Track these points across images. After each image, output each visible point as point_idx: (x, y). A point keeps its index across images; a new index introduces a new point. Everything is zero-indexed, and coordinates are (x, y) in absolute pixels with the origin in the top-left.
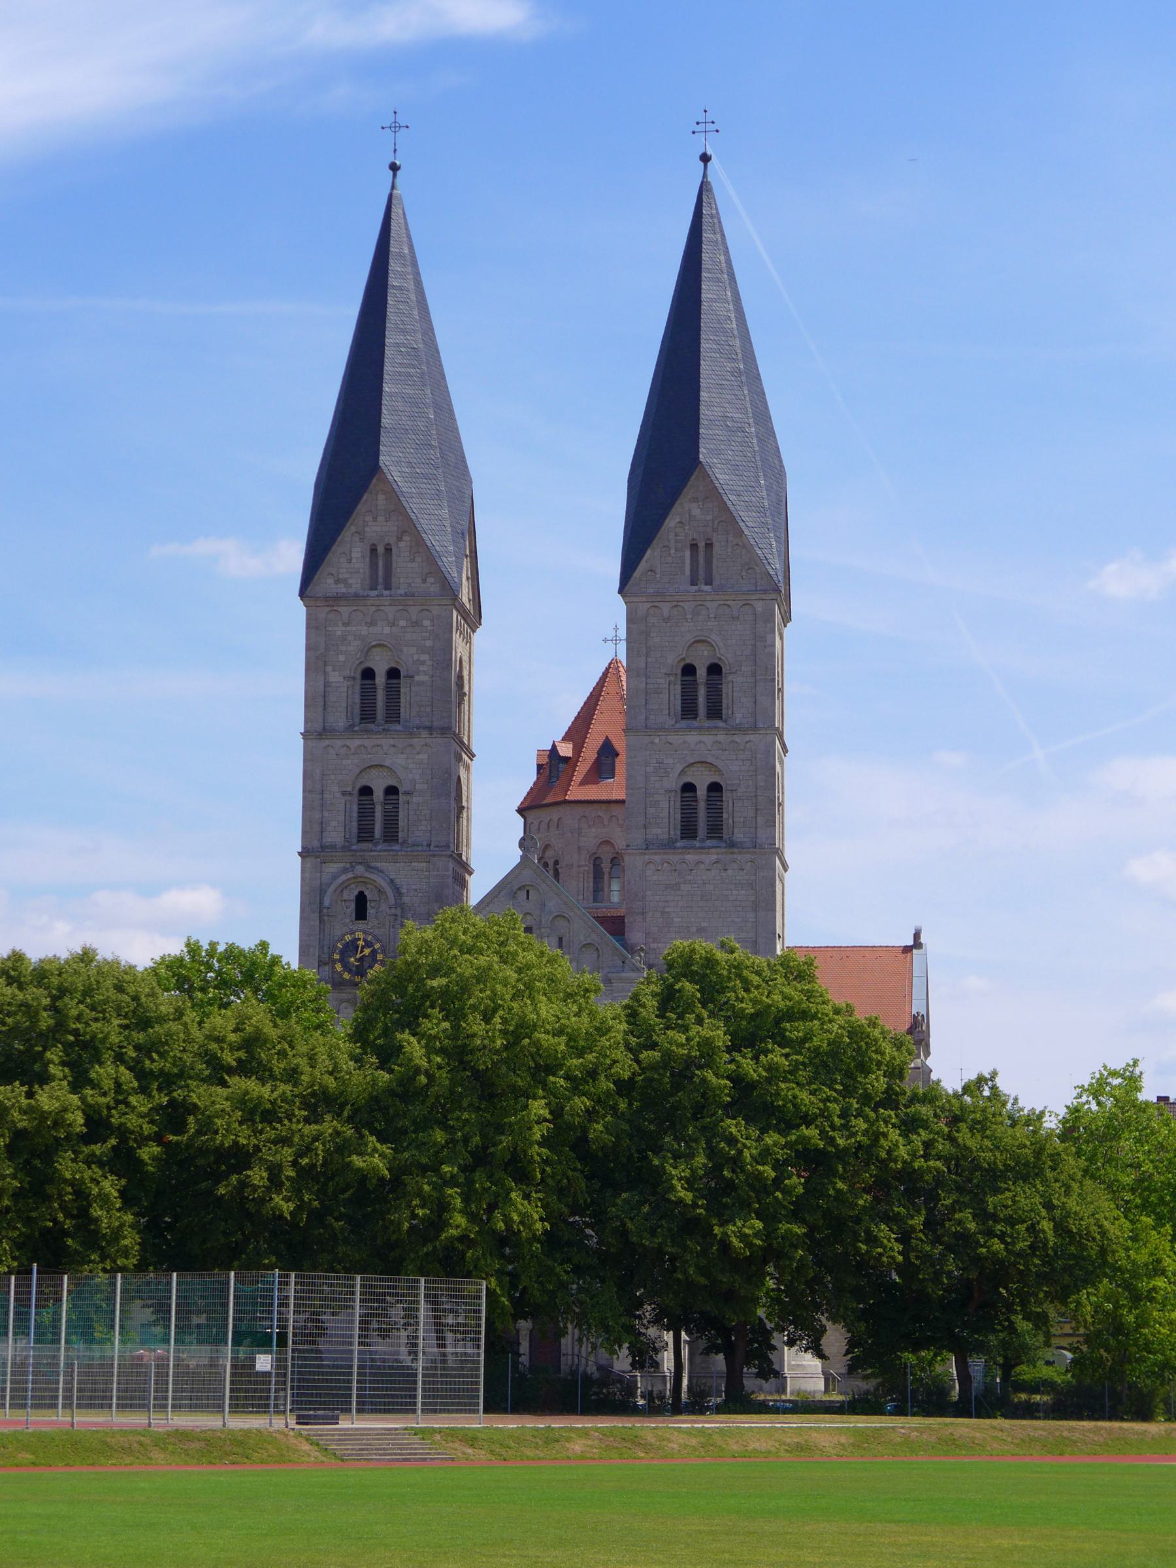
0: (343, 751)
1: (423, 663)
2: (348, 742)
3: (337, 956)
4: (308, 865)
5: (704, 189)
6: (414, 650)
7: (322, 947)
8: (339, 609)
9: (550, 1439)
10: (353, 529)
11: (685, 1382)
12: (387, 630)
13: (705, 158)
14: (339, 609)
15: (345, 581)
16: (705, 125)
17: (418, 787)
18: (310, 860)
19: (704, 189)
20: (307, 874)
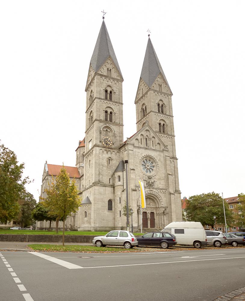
2: (104, 101)
12: (111, 83)
13: (149, 35)
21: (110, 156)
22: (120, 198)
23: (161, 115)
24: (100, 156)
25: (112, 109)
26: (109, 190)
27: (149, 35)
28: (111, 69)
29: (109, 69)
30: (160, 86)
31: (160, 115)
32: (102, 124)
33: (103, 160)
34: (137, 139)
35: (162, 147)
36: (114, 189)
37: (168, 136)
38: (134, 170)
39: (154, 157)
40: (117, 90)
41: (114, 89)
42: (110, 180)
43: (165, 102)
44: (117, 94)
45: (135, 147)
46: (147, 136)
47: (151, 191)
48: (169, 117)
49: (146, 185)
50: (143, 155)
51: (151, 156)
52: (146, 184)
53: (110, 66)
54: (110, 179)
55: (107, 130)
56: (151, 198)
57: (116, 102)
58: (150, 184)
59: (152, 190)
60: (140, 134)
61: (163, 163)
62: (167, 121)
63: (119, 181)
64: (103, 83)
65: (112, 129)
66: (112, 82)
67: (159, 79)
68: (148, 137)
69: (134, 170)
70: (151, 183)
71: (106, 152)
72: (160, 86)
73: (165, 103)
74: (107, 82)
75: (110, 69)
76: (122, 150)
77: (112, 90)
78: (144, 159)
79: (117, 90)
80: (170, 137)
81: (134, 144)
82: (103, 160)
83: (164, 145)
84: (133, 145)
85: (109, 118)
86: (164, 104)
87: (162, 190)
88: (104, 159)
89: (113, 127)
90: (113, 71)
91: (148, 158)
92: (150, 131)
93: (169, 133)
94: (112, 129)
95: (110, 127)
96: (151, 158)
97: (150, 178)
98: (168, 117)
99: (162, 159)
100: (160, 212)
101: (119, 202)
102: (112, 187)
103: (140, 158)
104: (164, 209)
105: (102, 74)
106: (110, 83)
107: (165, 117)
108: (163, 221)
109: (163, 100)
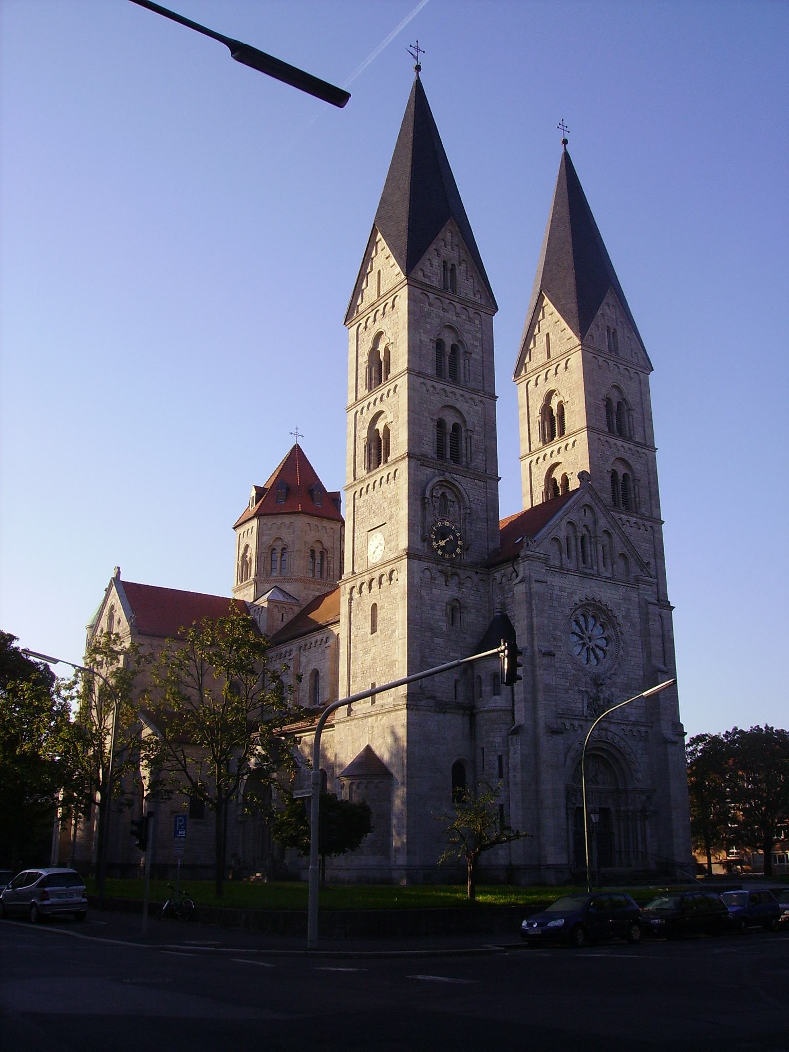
0: (431, 389)
1: (476, 347)
2: (435, 384)
3: (458, 550)
4: (413, 464)
5: (566, 156)
6: (470, 336)
7: (423, 528)
8: (429, 294)
9: (366, 618)
10: (434, 247)
11: (448, 664)
12: (455, 318)
13: (565, 142)
14: (429, 294)
15: (429, 277)
16: (562, 126)
17: (477, 428)
18: (413, 461)
19: (566, 156)
20: (412, 471)
21: (457, 595)
22: (500, 757)
23: (619, 443)
24: (424, 592)
25: (457, 411)
26: (456, 722)
27: (565, 142)
28: (456, 264)
29: (449, 266)
30: (612, 334)
31: (622, 446)
32: (429, 471)
33: (433, 608)
34: (555, 539)
35: (635, 570)
36: (473, 724)
37: (640, 522)
38: (550, 654)
39: (610, 605)
40: (477, 343)
41: (467, 338)
42: (459, 688)
43: (630, 390)
44: (475, 359)
45: (550, 569)
46: (585, 526)
47: (604, 733)
48: (644, 451)
49: (585, 709)
50: (576, 599)
51: (604, 608)
52: (585, 705)
53: (451, 253)
54: (456, 681)
55: (443, 494)
56: (602, 757)
57: (475, 391)
58: (599, 706)
59: (606, 730)
60: (564, 522)
61: (638, 628)
62: (637, 466)
63: (247, 546)
64: (429, 314)
65: (462, 490)
66: (457, 315)
67: (606, 307)
68: (588, 531)
69: (550, 654)
70: (601, 702)
71: (443, 579)
72: (612, 334)
73: (630, 399)
74: (441, 313)
75: (453, 265)
76: (498, 575)
77: (459, 341)
78: (577, 612)
79: (477, 343)
80: (648, 524)
81: (547, 559)
82: (433, 608)
83: (639, 560)
84: (546, 561)
85: (449, 450)
86: (624, 400)
87: (630, 727)
88: (438, 608)
89: (464, 484)
90: (461, 270)
91: (591, 609)
92: (596, 509)
93: (643, 510)
94: (462, 496)
95: (456, 483)
96: (599, 609)
97: (597, 682)
98: (639, 449)
99: (635, 613)
100: (631, 808)
101: (496, 772)
102: (463, 715)
103: (567, 611)
104: (644, 797)
105: (427, 281)
106: (451, 317)
107: (630, 449)
108: (640, 838)
109: (622, 386)
